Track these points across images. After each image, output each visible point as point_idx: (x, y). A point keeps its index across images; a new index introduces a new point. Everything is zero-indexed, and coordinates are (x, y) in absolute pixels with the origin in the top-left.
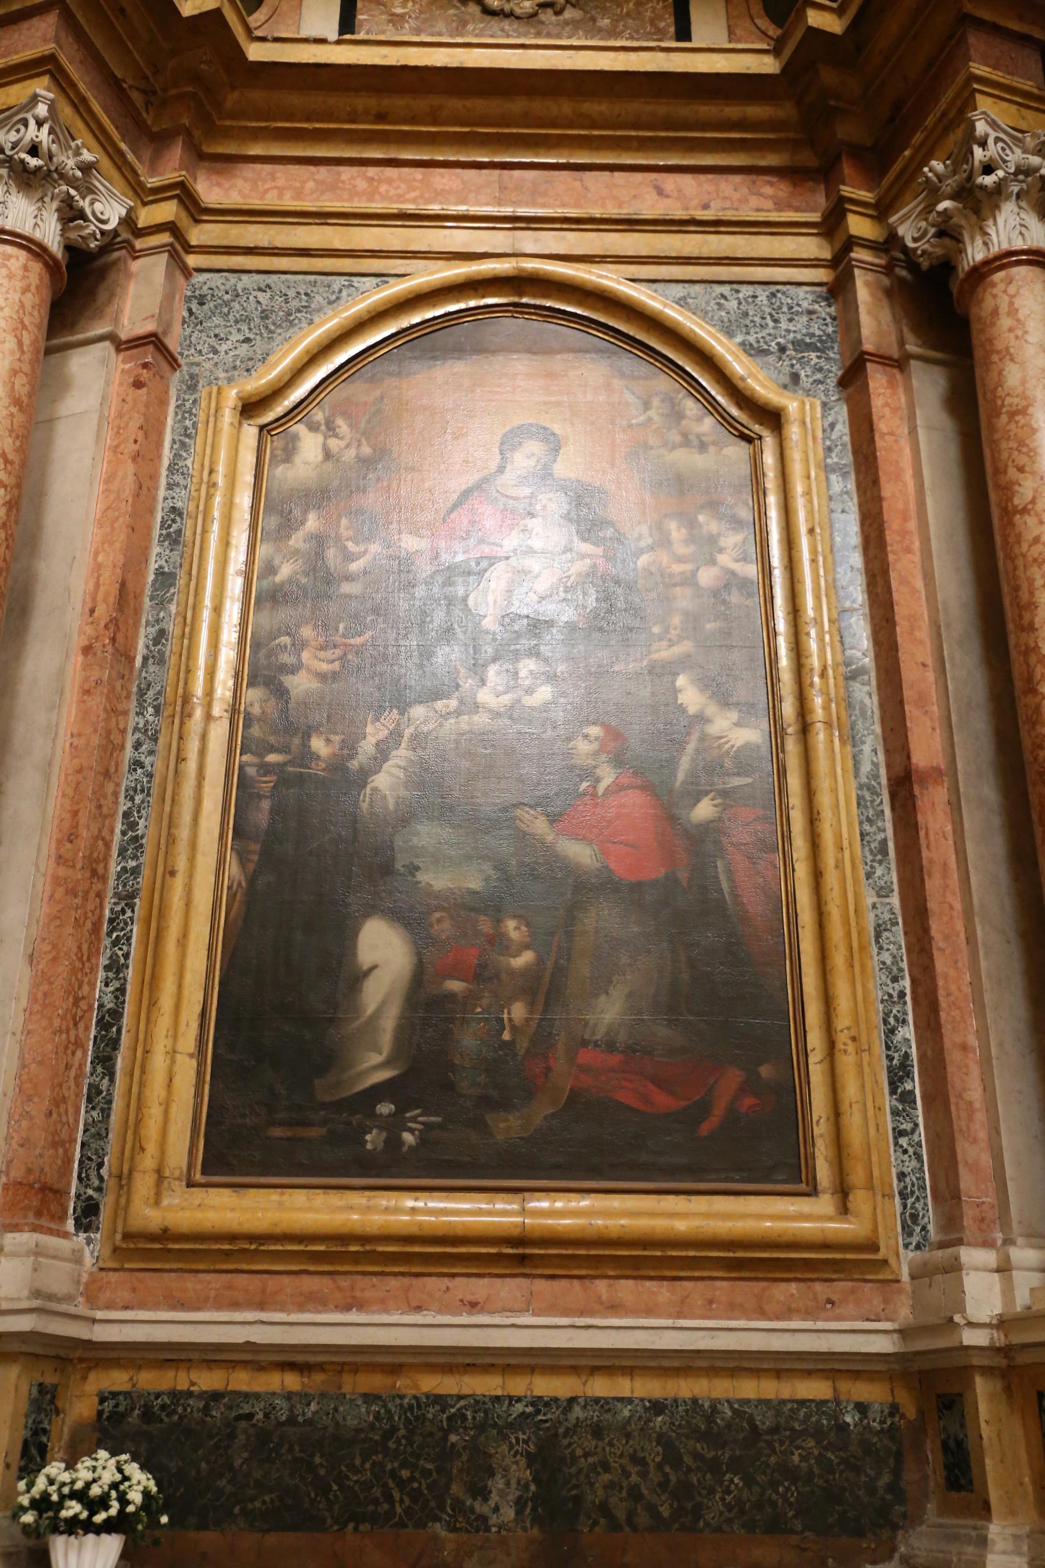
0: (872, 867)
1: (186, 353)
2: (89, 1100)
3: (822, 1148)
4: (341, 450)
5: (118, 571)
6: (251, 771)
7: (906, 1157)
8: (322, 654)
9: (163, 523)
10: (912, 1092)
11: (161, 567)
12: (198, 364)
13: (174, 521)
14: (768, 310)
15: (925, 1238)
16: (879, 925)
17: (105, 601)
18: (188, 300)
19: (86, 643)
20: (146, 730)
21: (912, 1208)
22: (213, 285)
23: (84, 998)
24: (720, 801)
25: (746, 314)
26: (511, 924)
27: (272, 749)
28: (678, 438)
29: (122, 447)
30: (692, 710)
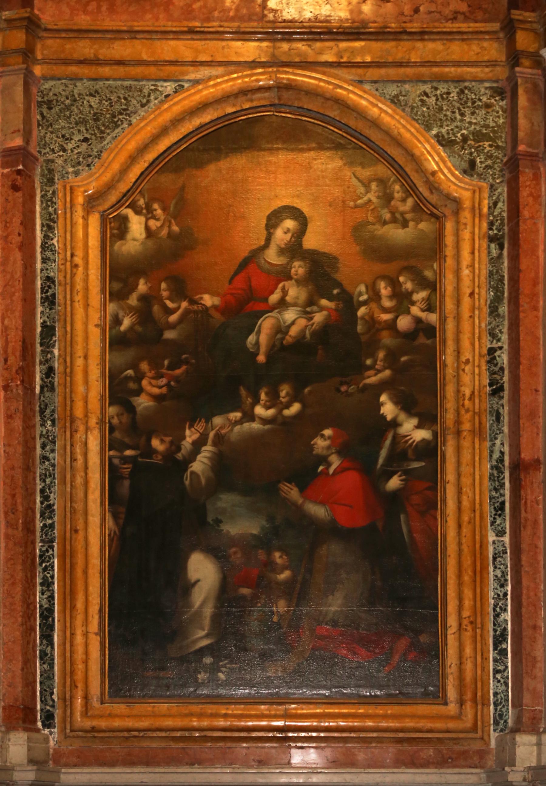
0: (495, 518)
1: (43, 151)
2: (41, 659)
3: (452, 680)
4: (158, 228)
5: (20, 333)
6: (116, 461)
7: (499, 684)
8: (154, 382)
9: (42, 289)
10: (506, 649)
11: (45, 322)
12: (53, 161)
13: (50, 287)
14: (457, 105)
15: (505, 726)
16: (495, 554)
17: (13, 353)
18: (40, 104)
19: (5, 383)
20: (48, 436)
21: (500, 710)
22: (56, 91)
23: (31, 603)
24: (403, 477)
25: (441, 109)
26: (277, 554)
27: (129, 447)
28: (387, 216)
29: (10, 237)
30: (389, 417)
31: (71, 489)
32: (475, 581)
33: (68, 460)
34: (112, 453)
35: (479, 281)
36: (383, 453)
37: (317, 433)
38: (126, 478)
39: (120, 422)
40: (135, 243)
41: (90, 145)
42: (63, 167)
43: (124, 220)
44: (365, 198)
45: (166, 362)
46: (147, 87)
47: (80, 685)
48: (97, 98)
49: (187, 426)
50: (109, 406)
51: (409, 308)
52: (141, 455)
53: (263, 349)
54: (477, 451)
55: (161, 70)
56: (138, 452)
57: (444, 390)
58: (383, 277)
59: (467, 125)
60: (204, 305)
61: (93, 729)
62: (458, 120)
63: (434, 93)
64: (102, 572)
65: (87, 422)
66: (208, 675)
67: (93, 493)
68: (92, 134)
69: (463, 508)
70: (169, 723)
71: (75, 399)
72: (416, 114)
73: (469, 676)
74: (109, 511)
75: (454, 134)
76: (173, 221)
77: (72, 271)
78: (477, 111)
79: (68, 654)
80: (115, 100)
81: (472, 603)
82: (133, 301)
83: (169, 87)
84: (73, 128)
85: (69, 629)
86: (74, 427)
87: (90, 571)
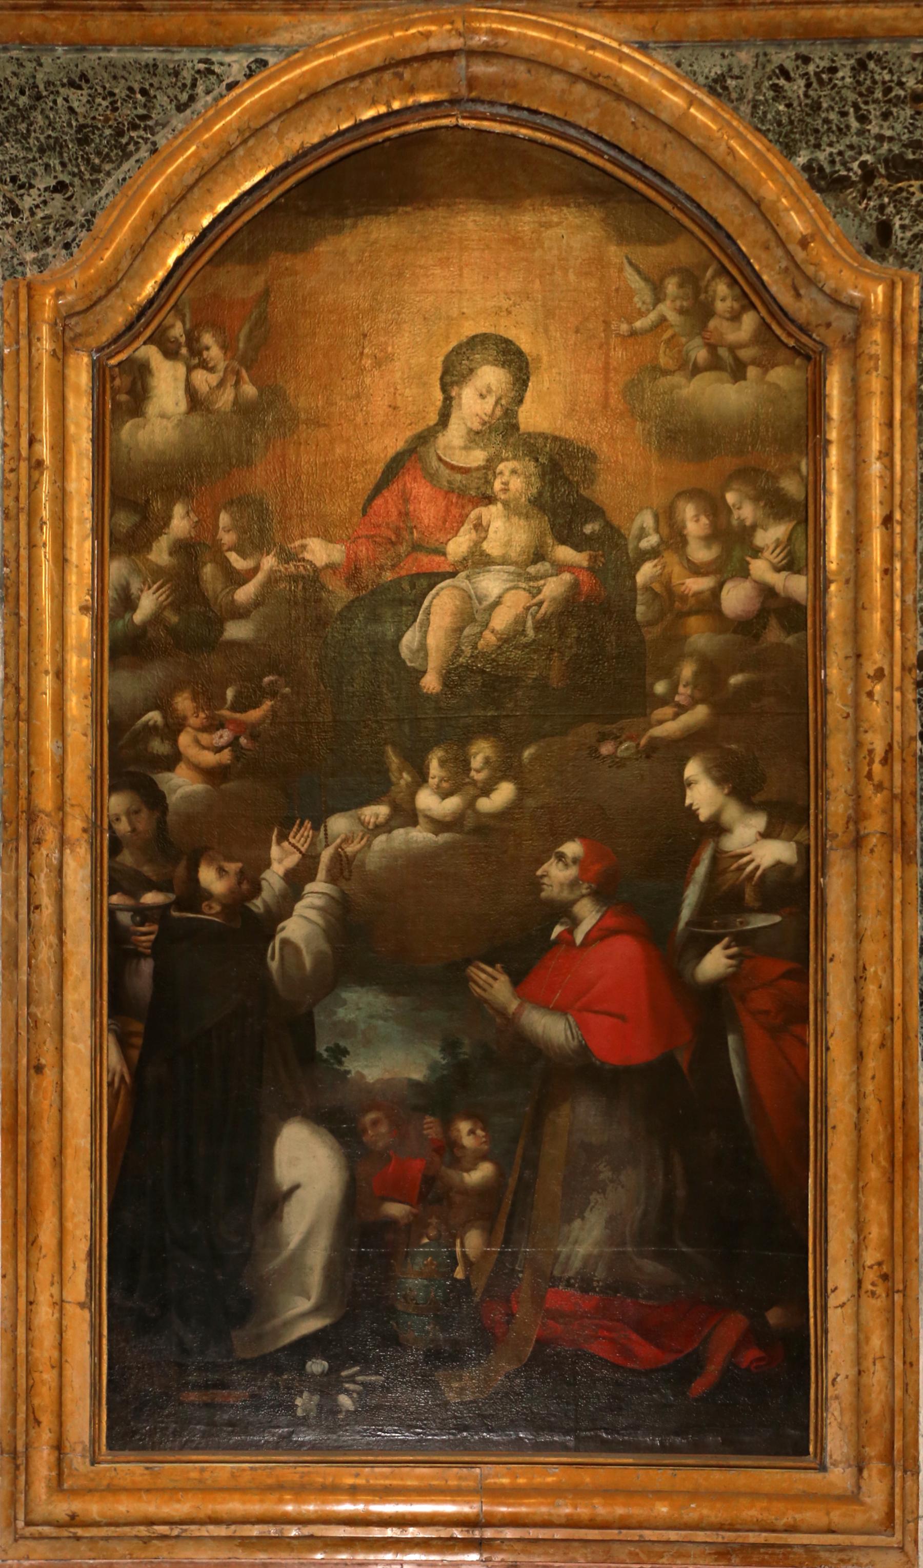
3: (837, 1413)
6: (125, 918)
8: (204, 738)
14: (851, 96)
25: (816, 107)
26: (464, 1127)
28: (701, 355)
30: (704, 814)
31: (29, 975)
32: (892, 1182)
33: (24, 910)
34: (115, 899)
35: (902, 495)
36: (692, 895)
37: (549, 851)
38: (145, 956)
39: (134, 830)
40: (165, 422)
41: (69, 199)
42: (12, 249)
43: (140, 373)
44: (653, 316)
45: (230, 693)
46: (189, 65)
47: (47, 1419)
48: (85, 92)
49: (274, 838)
50: (110, 795)
51: (748, 563)
52: (179, 904)
53: (434, 663)
54: (898, 884)
55: (219, 24)
56: (172, 897)
57: (824, 750)
58: (694, 494)
59: (873, 142)
60: (311, 563)
61: (73, 1520)
62: (853, 130)
63: (801, 71)
64: (94, 1167)
65: (63, 824)
66: (316, 1398)
67: (75, 988)
68: (74, 175)
69: (868, 1012)
70: (235, 1506)
71: (36, 769)
72: (763, 120)
73: (876, 1403)
74: (109, 1030)
75: (844, 164)
76: (244, 373)
77: (30, 477)
78: (894, 110)
79: (21, 1350)
80: (123, 95)
81: (886, 1231)
82: (160, 554)
83: (235, 63)
84: (34, 160)
85: (24, 1294)
86: (34, 834)
87: (70, 1164)
